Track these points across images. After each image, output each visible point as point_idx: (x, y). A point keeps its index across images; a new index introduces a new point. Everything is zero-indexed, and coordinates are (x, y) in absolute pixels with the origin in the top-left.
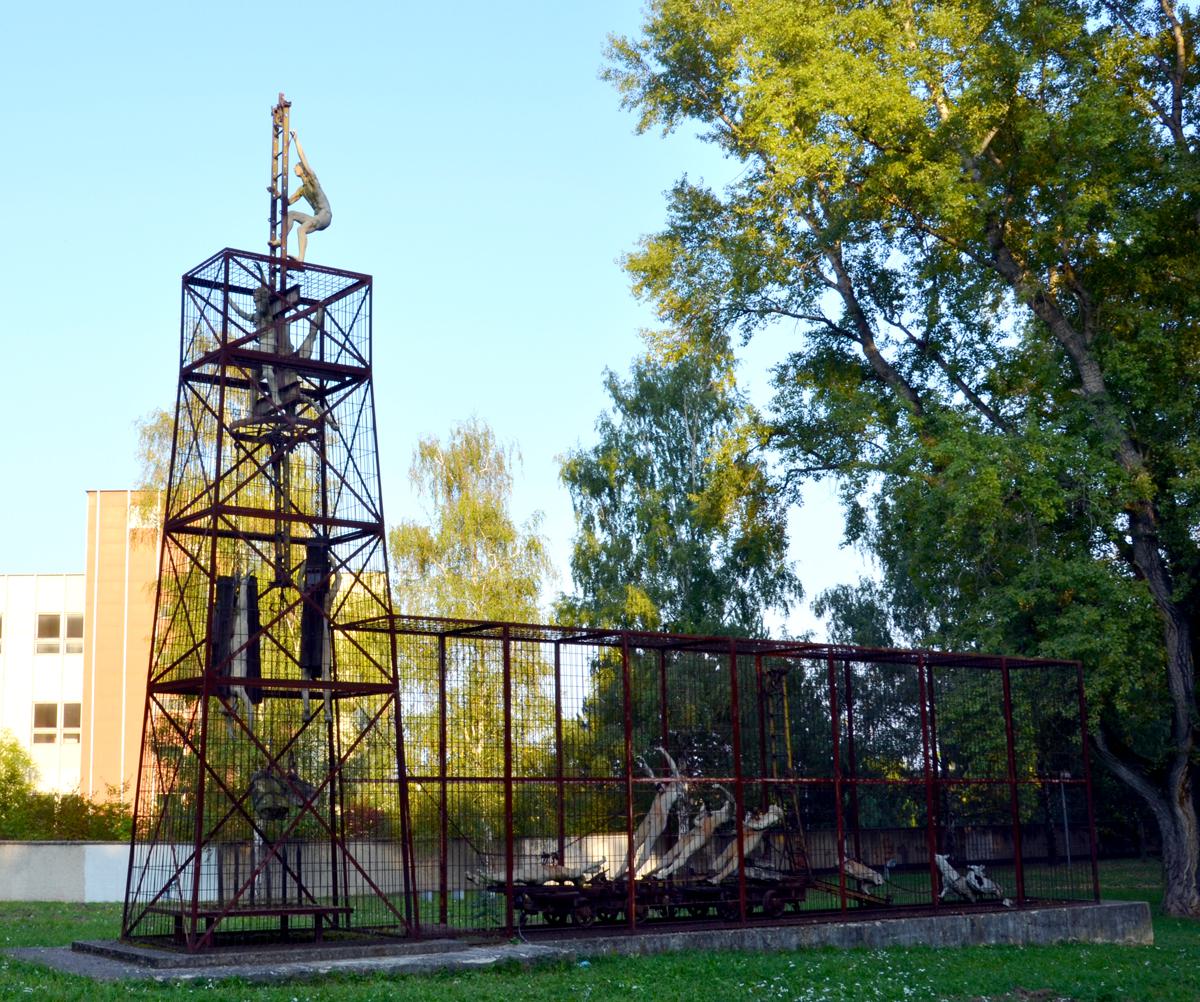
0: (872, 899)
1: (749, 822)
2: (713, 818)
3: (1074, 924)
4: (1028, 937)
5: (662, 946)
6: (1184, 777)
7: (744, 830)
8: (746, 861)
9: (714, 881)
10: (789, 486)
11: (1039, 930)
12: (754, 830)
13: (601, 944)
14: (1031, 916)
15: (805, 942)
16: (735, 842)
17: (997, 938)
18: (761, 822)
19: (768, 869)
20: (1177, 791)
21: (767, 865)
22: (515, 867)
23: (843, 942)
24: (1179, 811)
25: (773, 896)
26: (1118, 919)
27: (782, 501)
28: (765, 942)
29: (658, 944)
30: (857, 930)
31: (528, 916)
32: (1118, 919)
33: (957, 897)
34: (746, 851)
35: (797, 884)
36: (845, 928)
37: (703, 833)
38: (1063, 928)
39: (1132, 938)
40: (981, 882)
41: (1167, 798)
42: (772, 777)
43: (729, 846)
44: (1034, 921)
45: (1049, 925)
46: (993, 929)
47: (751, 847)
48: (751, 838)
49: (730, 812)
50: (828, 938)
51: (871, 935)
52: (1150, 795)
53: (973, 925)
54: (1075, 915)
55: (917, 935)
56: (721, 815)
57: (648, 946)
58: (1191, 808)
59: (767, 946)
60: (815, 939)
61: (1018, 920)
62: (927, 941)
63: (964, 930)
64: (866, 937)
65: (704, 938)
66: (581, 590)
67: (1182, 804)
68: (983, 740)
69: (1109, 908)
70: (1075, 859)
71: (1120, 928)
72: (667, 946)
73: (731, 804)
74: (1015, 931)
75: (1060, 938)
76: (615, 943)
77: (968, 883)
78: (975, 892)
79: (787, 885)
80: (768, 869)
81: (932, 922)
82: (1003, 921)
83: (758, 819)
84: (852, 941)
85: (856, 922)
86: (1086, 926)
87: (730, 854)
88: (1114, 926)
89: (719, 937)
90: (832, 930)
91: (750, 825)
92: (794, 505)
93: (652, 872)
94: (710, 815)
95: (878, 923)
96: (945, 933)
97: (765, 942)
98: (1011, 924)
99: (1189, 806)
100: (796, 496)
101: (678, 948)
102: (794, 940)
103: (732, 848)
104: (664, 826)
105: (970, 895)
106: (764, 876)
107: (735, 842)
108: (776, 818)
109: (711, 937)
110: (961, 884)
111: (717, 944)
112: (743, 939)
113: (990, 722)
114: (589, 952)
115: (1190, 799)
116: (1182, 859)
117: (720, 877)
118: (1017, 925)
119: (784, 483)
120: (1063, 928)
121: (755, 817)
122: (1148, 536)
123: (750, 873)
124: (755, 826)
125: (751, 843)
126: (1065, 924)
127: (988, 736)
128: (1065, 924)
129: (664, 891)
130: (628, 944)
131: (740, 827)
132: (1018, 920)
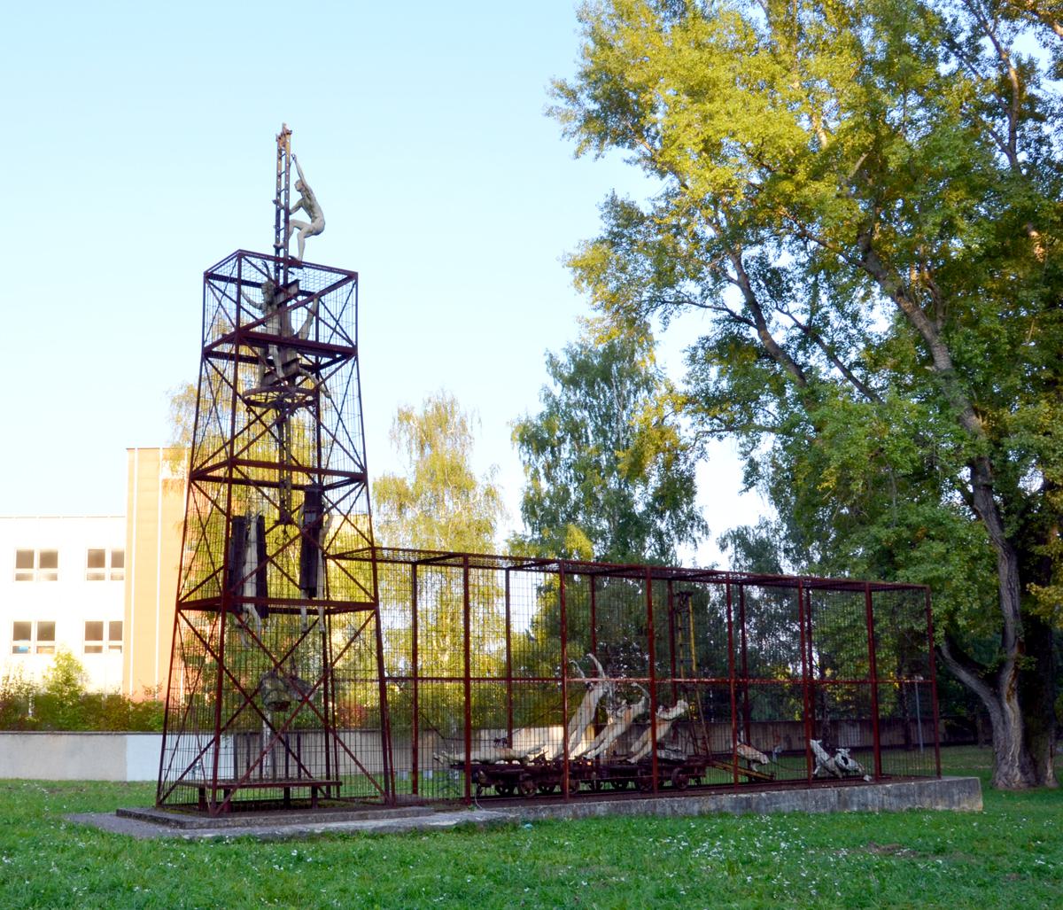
3: (920, 794)
7: (657, 720)
8: (658, 745)
12: (665, 720)
13: (541, 811)
14: (886, 789)
15: (705, 809)
16: (649, 730)
17: (858, 807)
20: (1005, 690)
24: (1007, 706)
25: (679, 772)
28: (672, 809)
29: (587, 811)
30: (747, 799)
32: (955, 791)
35: (699, 763)
38: (912, 798)
39: (966, 805)
40: (846, 762)
41: (997, 695)
44: (888, 793)
45: (900, 796)
46: (855, 799)
47: (663, 734)
49: (646, 706)
51: (758, 804)
52: (983, 693)
56: (638, 708)
60: (713, 807)
63: (832, 800)
64: (754, 805)
67: (1009, 700)
71: (956, 798)
73: (647, 699)
75: (909, 806)
76: (552, 810)
77: (836, 763)
78: (842, 770)
81: (806, 793)
82: (863, 793)
86: (930, 796)
89: (636, 805)
91: (662, 716)
92: (701, 460)
95: (763, 794)
96: (817, 802)
97: (672, 809)
98: (870, 795)
100: (703, 453)
102: (696, 807)
103: (647, 734)
106: (673, 756)
107: (649, 730)
109: (629, 805)
110: (830, 764)
112: (655, 807)
114: (532, 817)
115: (1016, 697)
116: (1008, 745)
118: (874, 795)
120: (912, 798)
121: (666, 709)
123: (661, 754)
124: (666, 717)
125: (662, 731)
130: (563, 810)
131: (653, 717)
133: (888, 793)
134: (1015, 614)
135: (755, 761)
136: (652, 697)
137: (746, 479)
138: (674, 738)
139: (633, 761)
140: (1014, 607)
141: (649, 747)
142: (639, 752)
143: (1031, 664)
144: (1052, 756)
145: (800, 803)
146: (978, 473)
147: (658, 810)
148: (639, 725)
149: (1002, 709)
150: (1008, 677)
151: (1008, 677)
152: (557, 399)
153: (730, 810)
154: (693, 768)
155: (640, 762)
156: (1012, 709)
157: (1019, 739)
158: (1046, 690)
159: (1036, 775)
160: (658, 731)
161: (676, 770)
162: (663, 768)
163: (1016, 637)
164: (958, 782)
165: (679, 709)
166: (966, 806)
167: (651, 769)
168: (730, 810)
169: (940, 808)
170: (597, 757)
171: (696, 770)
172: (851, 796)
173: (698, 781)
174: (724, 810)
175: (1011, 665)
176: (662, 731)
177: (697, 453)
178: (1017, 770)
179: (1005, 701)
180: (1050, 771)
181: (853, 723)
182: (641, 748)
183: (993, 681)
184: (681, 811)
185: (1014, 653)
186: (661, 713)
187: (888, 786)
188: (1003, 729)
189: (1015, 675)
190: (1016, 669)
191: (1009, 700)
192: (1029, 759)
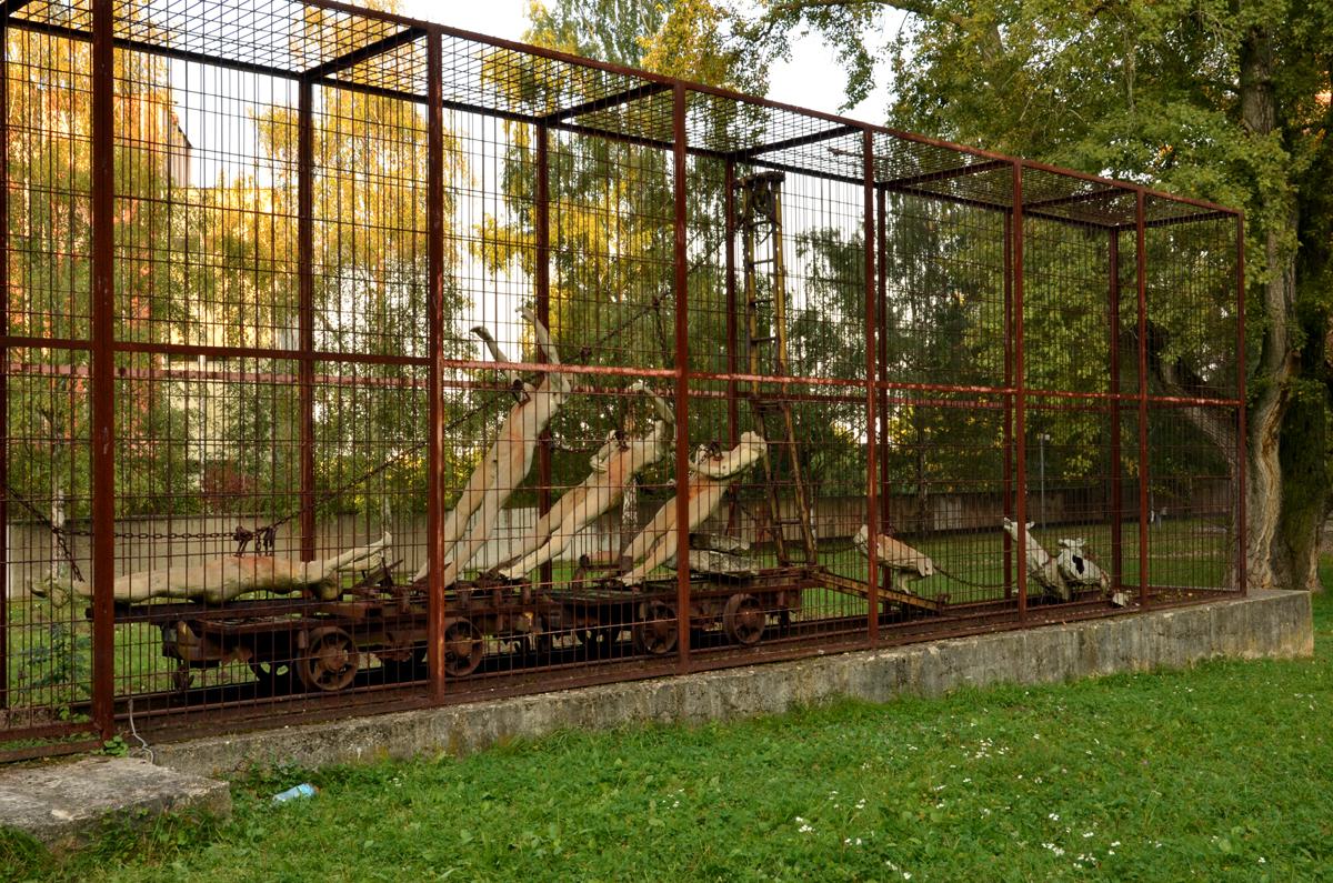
0: (913, 601)
1: (701, 463)
2: (628, 454)
3: (1220, 629)
4: (1158, 656)
5: (502, 729)
6: (1272, 419)
7: (692, 479)
8: (691, 540)
9: (628, 580)
10: (773, 32)
11: (1173, 642)
12: (711, 478)
13: (351, 737)
14: (1162, 622)
15: (803, 694)
16: (672, 503)
17: (1115, 663)
18: (725, 463)
19: (734, 554)
20: (1262, 436)
21: (735, 546)
22: (118, 565)
23: (872, 689)
24: (1261, 463)
25: (744, 604)
26: (1274, 619)
27: (764, 52)
28: (725, 701)
29: (493, 727)
30: (901, 665)
31: (195, 673)
32: (1274, 619)
33: (1042, 590)
34: (693, 521)
35: (786, 582)
36: (876, 663)
37: (604, 483)
38: (1205, 638)
39: (1289, 647)
40: (1080, 568)
41: (1248, 450)
42: (748, 372)
43: (660, 513)
44: (1167, 631)
45: (1186, 636)
46: (1110, 648)
47: (704, 513)
48: (704, 495)
49: (665, 443)
50: (846, 684)
51: (922, 673)
52: (1224, 440)
53: (1082, 642)
54: (1221, 615)
55: (996, 667)
56: (646, 449)
57: (468, 733)
58: (1276, 458)
59: (730, 710)
60: (822, 687)
61: (1146, 630)
62: (1013, 676)
63: (1068, 652)
64: (912, 678)
65: (598, 702)
66: (515, 217)
67: (1265, 453)
68: (1036, 362)
69: (1264, 603)
70: (1048, 525)
71: (1275, 632)
72: (514, 727)
73: (668, 426)
74: (1141, 649)
75: (1201, 654)
76: (386, 732)
77: (1060, 569)
78: (1071, 583)
79: (773, 584)
80: (734, 554)
81: (1020, 640)
82: (1125, 633)
83: (720, 459)
84: (889, 686)
85: (893, 647)
86: (1234, 633)
87: (660, 527)
88: (1268, 631)
89: (630, 699)
90: (854, 668)
91: (704, 469)
92: (779, 60)
93: (500, 566)
94: (623, 448)
95: (933, 650)
96: (1039, 659)
97: (725, 701)
98: (1135, 637)
99: (1274, 455)
100: (783, 49)
101: (538, 731)
102: (783, 693)
103: (667, 514)
104: (527, 470)
105: (1062, 588)
106: (728, 567)
107: (672, 503)
108: (755, 456)
109: (613, 701)
110: (1050, 573)
111: (625, 714)
112: (681, 700)
113: (1046, 335)
114: (318, 759)
115: (1277, 448)
116: (1258, 525)
117: (638, 571)
118: (1141, 637)
119: (768, 25)
120: (1205, 638)
121: (716, 450)
122: (1266, 83)
123: (701, 561)
124: (714, 470)
125: (703, 504)
126: (1207, 632)
127: (1044, 355)
128: (1207, 632)
129: (522, 605)
130: (420, 731)
131: (682, 471)
132: (1146, 630)
133: (1167, 631)
134: (1289, 312)
135: (904, 571)
136: (678, 421)
137: (851, 90)
138: (731, 523)
139: (628, 580)
140: (1287, 299)
141: (671, 544)
142: (642, 560)
143: (1314, 391)
144: (1317, 544)
145: (1007, 664)
146: (1256, 61)
147: (689, 708)
148: (655, 488)
149: (1254, 469)
150: (1268, 416)
151: (1268, 416)
152: (550, 13)
153: (861, 694)
154: (774, 593)
155: (646, 586)
156: (1268, 468)
157: (1275, 517)
158: (1315, 439)
159: (1294, 574)
160: (692, 505)
161: (736, 599)
162: (705, 596)
163: (1287, 350)
164: (1278, 602)
165: (747, 452)
166: (1289, 649)
167: (674, 599)
168: (861, 694)
169: (1249, 654)
170: (546, 569)
171: (781, 596)
172: (1102, 642)
173: (784, 617)
174: (847, 694)
175: (1276, 395)
176: (703, 504)
177: (771, 47)
178: (1266, 567)
179: (1260, 454)
180: (1313, 567)
181: (951, 498)
182: (654, 552)
183: (1241, 422)
184: (746, 705)
185: (1284, 374)
186: (701, 463)
187: (1166, 616)
188: (1253, 502)
189: (1279, 412)
190: (1282, 401)
191: (1265, 453)
192: (1285, 548)
